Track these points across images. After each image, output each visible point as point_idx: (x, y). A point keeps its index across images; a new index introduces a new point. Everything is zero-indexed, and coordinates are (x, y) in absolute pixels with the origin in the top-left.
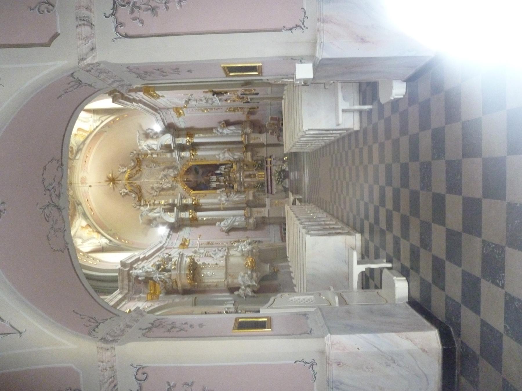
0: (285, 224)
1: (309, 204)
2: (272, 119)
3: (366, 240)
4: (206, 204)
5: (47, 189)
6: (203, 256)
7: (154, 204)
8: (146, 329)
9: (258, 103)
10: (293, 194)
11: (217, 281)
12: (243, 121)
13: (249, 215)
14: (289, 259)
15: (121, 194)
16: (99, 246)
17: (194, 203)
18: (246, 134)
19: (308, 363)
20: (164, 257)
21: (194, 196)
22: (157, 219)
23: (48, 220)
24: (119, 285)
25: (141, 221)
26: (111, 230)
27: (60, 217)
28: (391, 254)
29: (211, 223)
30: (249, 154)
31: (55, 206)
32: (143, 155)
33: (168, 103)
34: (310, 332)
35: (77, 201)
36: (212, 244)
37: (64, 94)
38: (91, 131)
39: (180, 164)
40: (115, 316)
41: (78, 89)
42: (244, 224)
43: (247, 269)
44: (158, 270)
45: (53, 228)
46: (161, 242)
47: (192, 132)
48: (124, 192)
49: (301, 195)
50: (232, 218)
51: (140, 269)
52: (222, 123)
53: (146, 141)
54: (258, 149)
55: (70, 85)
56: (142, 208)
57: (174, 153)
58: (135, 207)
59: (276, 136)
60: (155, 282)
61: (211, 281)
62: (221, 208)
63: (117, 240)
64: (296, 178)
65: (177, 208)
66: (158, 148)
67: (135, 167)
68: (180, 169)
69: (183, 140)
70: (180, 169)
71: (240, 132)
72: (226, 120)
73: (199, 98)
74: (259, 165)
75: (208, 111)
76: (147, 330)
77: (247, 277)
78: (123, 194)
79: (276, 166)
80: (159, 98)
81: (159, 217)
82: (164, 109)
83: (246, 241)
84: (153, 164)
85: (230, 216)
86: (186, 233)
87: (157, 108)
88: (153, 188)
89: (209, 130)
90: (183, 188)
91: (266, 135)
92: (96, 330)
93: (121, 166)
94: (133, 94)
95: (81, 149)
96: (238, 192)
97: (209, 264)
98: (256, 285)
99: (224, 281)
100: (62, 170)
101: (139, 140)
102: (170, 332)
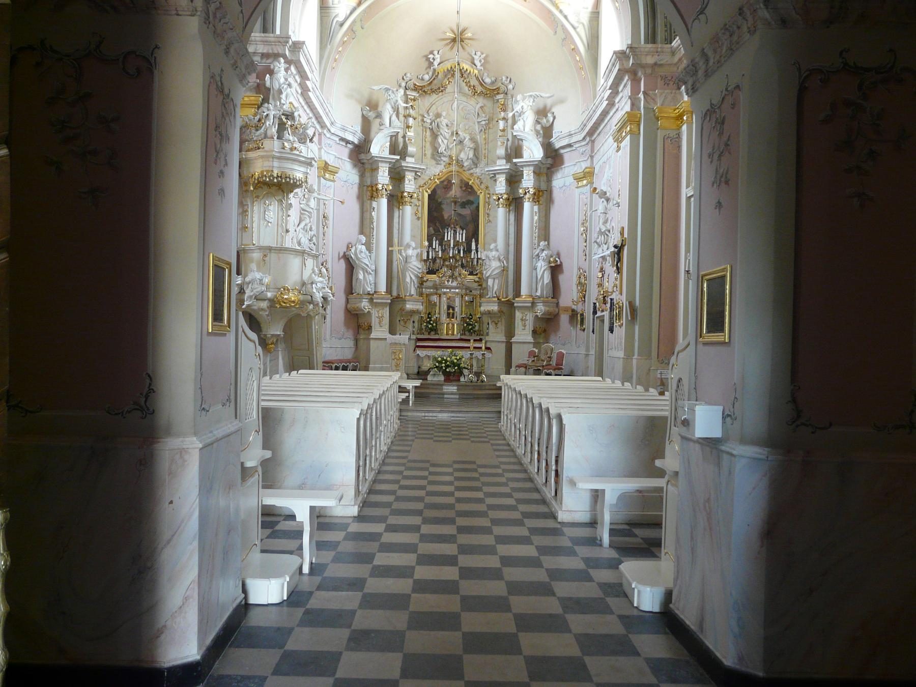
0: (355, 369)
2: (561, 356)
4: (402, 218)
6: (301, 206)
8: (222, 84)
9: (593, 331)
10: (416, 387)
13: (375, 301)
15: (432, 53)
17: (406, 194)
18: (533, 304)
19: (146, 401)
20: (308, 129)
22: (378, 120)
24: (257, 34)
25: (376, 88)
26: (362, 28)
29: (365, 225)
30: (495, 308)
32: (505, 101)
33: (604, 158)
39: (483, 172)
40: (245, 20)
42: (358, 289)
44: (283, 114)
46: (332, 124)
47: (542, 200)
48: (434, 59)
49: (414, 403)
50: (373, 267)
51: (286, 80)
52: (557, 259)
53: (531, 109)
54: (502, 327)
56: (402, 91)
57: (504, 161)
58: (403, 79)
59: (526, 362)
61: (255, 219)
62: (392, 246)
64: (445, 396)
65: (397, 160)
66: (517, 131)
67: (481, 84)
68: (472, 171)
69: (528, 181)
70: (472, 171)
71: (538, 294)
72: (562, 268)
74: (471, 325)
75: (582, 234)
76: (220, 85)
77: (258, 290)
78: (431, 56)
79: (471, 358)
81: (381, 124)
82: (592, 150)
83: (330, 291)
86: (348, 174)
87: (595, 136)
88: (438, 116)
89: (544, 232)
90: (435, 175)
93: (484, 59)
96: (422, 282)
97: (289, 216)
98: (244, 307)
99: (254, 245)
101: (536, 97)
102: (216, 131)
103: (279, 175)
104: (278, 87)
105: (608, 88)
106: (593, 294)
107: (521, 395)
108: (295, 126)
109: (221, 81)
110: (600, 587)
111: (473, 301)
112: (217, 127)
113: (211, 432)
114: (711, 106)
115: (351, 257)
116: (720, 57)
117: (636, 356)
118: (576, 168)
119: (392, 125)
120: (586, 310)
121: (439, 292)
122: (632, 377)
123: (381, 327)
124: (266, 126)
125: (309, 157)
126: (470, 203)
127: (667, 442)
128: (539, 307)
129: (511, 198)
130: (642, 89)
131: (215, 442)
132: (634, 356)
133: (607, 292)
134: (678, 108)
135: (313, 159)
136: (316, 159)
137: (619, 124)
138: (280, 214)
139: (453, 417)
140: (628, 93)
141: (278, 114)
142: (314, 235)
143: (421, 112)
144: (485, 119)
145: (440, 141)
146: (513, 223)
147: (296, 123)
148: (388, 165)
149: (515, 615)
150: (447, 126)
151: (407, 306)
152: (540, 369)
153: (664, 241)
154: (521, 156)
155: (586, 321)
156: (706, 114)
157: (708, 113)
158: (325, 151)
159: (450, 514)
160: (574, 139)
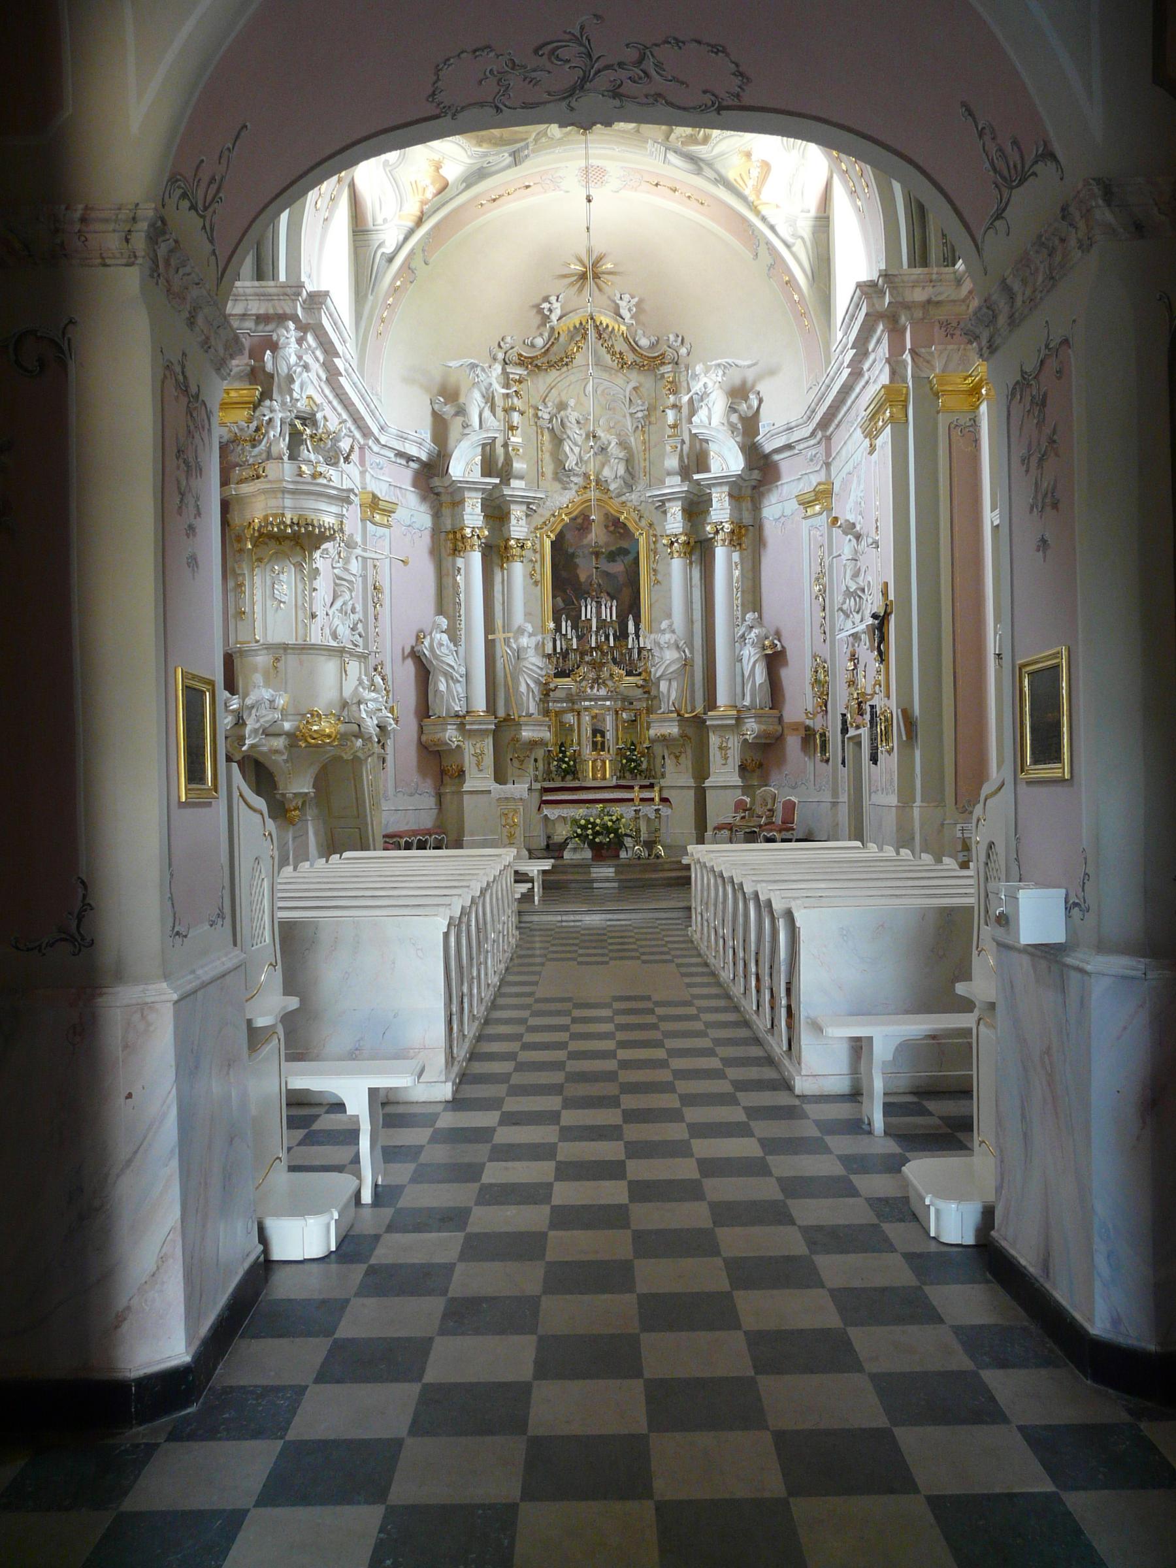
2: (790, 807)
3: (434, 1117)
4: (508, 584)
6: (336, 571)
8: (185, 377)
9: (843, 763)
10: (544, 872)
11: (259, 616)
13: (468, 727)
14: (335, 858)
15: (546, 299)
16: (374, 220)
17: (512, 542)
18: (739, 719)
20: (339, 441)
24: (248, 284)
25: (453, 364)
27: (545, 95)
28: (404, 1202)
30: (673, 730)
31: (585, 79)
32: (674, 377)
34: (178, 933)
35: (526, 152)
38: (759, 208)
39: (642, 498)
41: (991, 173)
42: (439, 709)
43: (299, 717)
44: (297, 418)
46: (382, 428)
48: (550, 310)
49: (543, 900)
50: (463, 670)
51: (300, 358)
52: (776, 642)
54: (687, 761)
55: (1008, 148)
56: (498, 368)
57: (677, 479)
59: (730, 820)
60: (256, 406)
61: (258, 597)
62: (493, 633)
63: (395, 279)
65: (496, 486)
66: (697, 427)
67: (634, 350)
68: (623, 498)
69: (721, 510)
70: (623, 498)
74: (634, 761)
76: (181, 378)
78: (546, 305)
79: (637, 818)
81: (466, 426)
83: (390, 715)
87: (831, 429)
88: (562, 406)
90: (561, 508)
92: (186, 204)
93: (637, 305)
94: (883, 350)
95: (699, 172)
96: (546, 692)
97: (315, 590)
98: (244, 748)
99: (257, 641)
100: (703, 109)
101: (725, 367)
102: (178, 458)
103: (295, 521)
104: (286, 371)
105: (850, 346)
106: (841, 699)
108: (318, 437)
109: (183, 373)
113: (193, 972)
114: (1022, 376)
116: (1034, 291)
117: (918, 803)
119: (484, 426)
122: (913, 839)
124: (269, 438)
126: (623, 552)
127: (975, 952)
128: (748, 726)
130: (909, 346)
131: (200, 989)
133: (864, 694)
134: (970, 376)
135: (352, 490)
136: (356, 491)
137: (872, 407)
138: (300, 586)
140: (885, 354)
141: (287, 417)
143: (533, 402)
145: (567, 449)
147: (320, 431)
148: (479, 495)
150: (578, 422)
152: (755, 832)
154: (707, 469)
155: (830, 746)
156: (1014, 388)
159: (611, 1089)
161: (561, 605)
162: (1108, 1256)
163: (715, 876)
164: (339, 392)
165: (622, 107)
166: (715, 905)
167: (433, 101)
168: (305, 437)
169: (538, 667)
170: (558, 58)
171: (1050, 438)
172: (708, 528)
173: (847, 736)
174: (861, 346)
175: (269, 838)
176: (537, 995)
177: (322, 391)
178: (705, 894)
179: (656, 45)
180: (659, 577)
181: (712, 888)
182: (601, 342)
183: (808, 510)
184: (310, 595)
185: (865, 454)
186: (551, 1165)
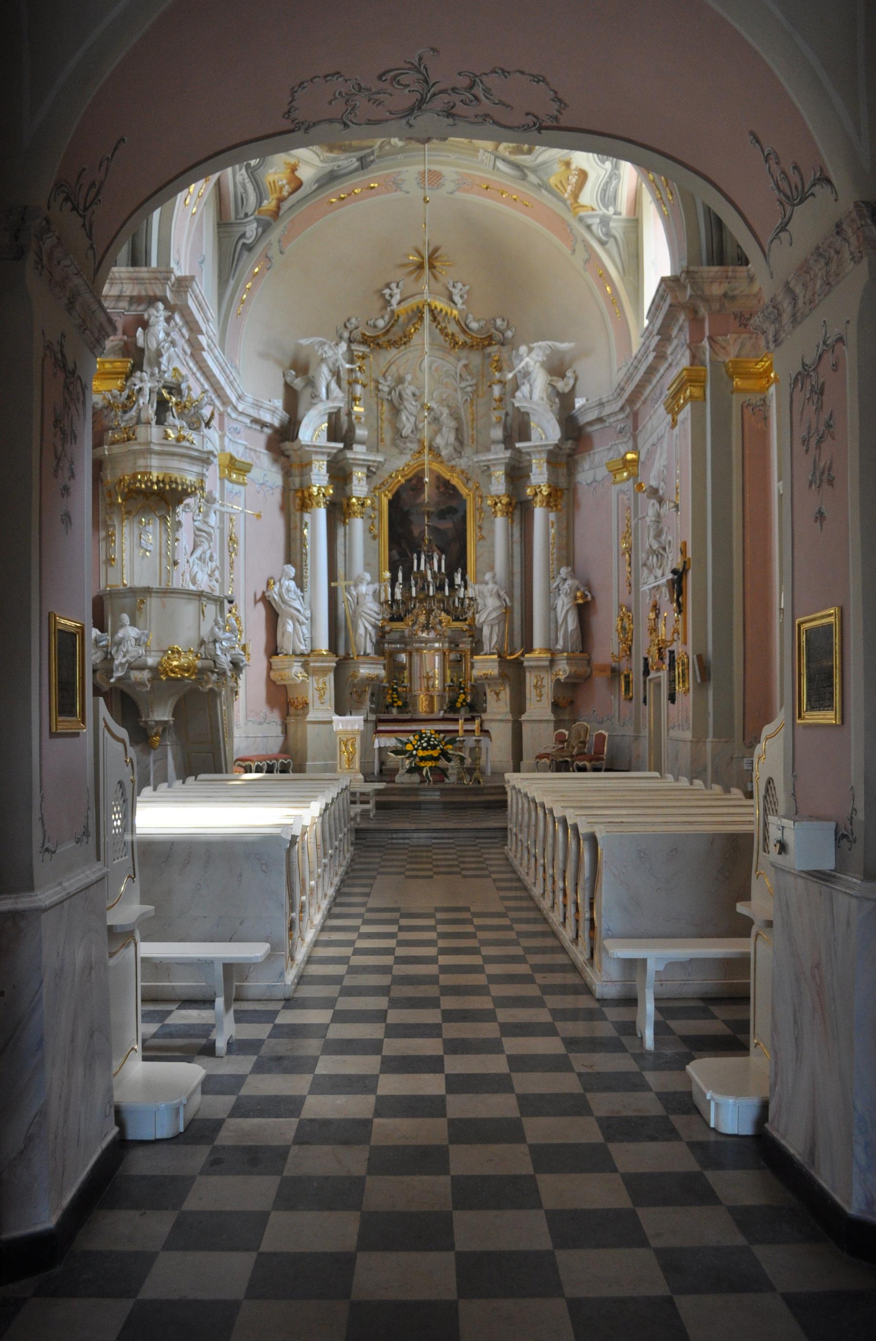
1: (352, 844)
4: (349, 538)
5: (475, 81)
6: (196, 523)
7: (352, 383)
8: (63, 355)
9: (645, 702)
12: (589, 655)
15: (388, 286)
17: (354, 500)
18: (552, 662)
20: (202, 408)
21: (372, 504)
22: (309, 390)
23: (384, 78)
24: (123, 269)
25: (304, 342)
26: (282, 253)
27: (387, 114)
31: (422, 101)
35: (372, 158)
36: (233, 551)
37: (763, 152)
39: (470, 463)
40: (97, 260)
41: (776, 192)
43: (162, 654)
44: (164, 387)
45: (360, 91)
46: (240, 398)
47: (562, 503)
48: (391, 296)
50: (308, 613)
51: (168, 334)
52: (587, 593)
54: (506, 694)
55: (790, 172)
56: (344, 346)
60: (128, 376)
67: (464, 331)
68: (453, 463)
70: (453, 463)
73: (666, 529)
75: (623, 554)
76: (59, 356)
77: (134, 654)
78: (387, 291)
80: (668, 413)
83: (242, 653)
84: (471, 386)
85: (312, 607)
88: (400, 380)
90: (398, 471)
91: (548, 721)
93: (468, 292)
94: (686, 336)
96: (382, 634)
97: (177, 540)
98: (112, 680)
100: (526, 128)
102: (55, 426)
103: (161, 478)
104: (155, 345)
105: (655, 332)
106: (644, 646)
107: (536, 804)
108: (183, 405)
109: (61, 352)
110: (660, 1099)
111: (460, 661)
112: (57, 422)
113: (60, 884)
114: (803, 367)
115: (274, 599)
116: (813, 295)
117: (710, 739)
118: (611, 454)
119: (331, 397)
120: (633, 669)
121: (409, 648)
122: (705, 770)
123: (323, 703)
124: (139, 405)
125: (205, 449)
126: (452, 511)
127: (754, 876)
128: (561, 667)
129: (514, 502)
130: (707, 333)
131: (66, 899)
132: (707, 737)
133: (664, 641)
134: (761, 361)
135: (211, 453)
136: (216, 453)
137: (674, 386)
138: (164, 537)
139: (435, 838)
140: (686, 340)
141: (155, 387)
142: (217, 567)
143: (374, 376)
144: (472, 383)
145: (404, 418)
146: (519, 540)
147: (185, 399)
148: (325, 458)
149: (531, 1147)
150: (414, 395)
151: (362, 671)
152: (567, 761)
153: (748, 563)
154: (528, 438)
155: (633, 687)
156: (796, 378)
157: (799, 377)
158: (230, 440)
159: (432, 991)
160: (607, 410)
161: (396, 556)
162: (866, 1147)
163: (529, 802)
164: (202, 364)
165: (455, 125)
166: (528, 827)
167: (288, 118)
168: (170, 404)
169: (375, 612)
170: (399, 83)
171: (828, 423)
172: (528, 491)
173: (649, 678)
174: (664, 334)
175: (130, 765)
176: (369, 905)
177: (187, 364)
178: (520, 817)
179: (485, 74)
180: (484, 533)
181: (526, 812)
182: (435, 324)
183: (617, 476)
184: (173, 544)
185: (668, 428)
186: (377, 1059)
